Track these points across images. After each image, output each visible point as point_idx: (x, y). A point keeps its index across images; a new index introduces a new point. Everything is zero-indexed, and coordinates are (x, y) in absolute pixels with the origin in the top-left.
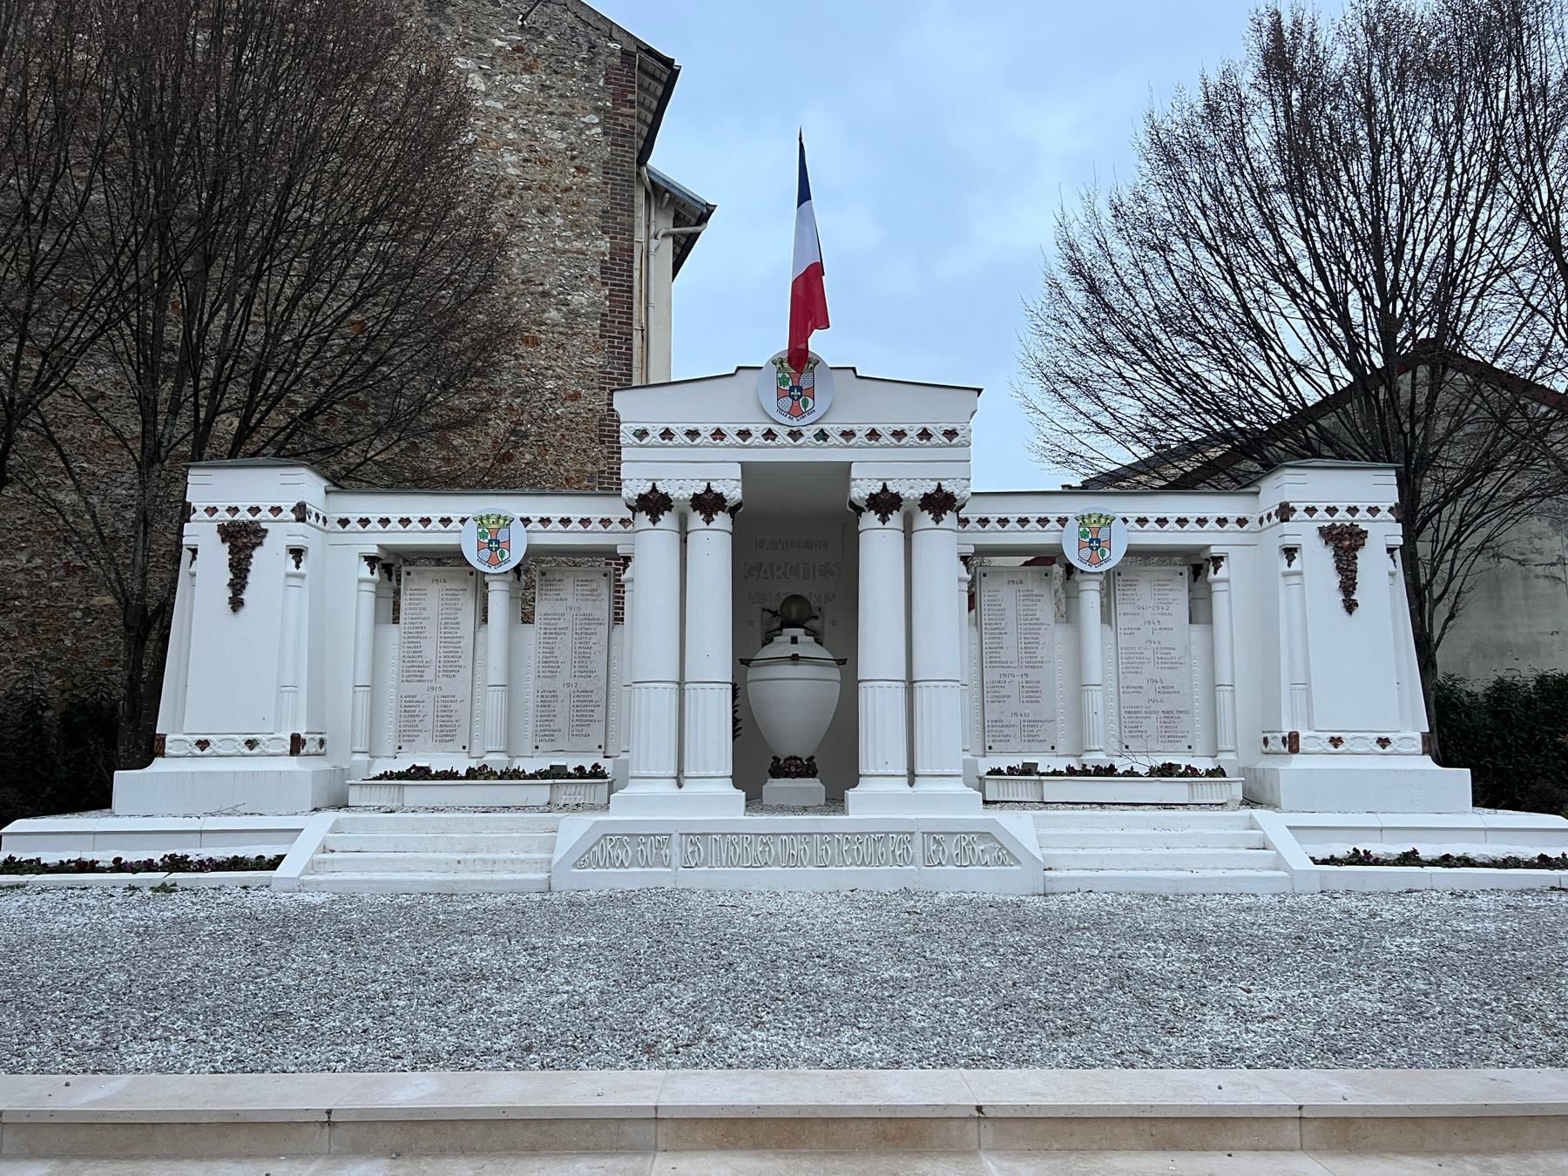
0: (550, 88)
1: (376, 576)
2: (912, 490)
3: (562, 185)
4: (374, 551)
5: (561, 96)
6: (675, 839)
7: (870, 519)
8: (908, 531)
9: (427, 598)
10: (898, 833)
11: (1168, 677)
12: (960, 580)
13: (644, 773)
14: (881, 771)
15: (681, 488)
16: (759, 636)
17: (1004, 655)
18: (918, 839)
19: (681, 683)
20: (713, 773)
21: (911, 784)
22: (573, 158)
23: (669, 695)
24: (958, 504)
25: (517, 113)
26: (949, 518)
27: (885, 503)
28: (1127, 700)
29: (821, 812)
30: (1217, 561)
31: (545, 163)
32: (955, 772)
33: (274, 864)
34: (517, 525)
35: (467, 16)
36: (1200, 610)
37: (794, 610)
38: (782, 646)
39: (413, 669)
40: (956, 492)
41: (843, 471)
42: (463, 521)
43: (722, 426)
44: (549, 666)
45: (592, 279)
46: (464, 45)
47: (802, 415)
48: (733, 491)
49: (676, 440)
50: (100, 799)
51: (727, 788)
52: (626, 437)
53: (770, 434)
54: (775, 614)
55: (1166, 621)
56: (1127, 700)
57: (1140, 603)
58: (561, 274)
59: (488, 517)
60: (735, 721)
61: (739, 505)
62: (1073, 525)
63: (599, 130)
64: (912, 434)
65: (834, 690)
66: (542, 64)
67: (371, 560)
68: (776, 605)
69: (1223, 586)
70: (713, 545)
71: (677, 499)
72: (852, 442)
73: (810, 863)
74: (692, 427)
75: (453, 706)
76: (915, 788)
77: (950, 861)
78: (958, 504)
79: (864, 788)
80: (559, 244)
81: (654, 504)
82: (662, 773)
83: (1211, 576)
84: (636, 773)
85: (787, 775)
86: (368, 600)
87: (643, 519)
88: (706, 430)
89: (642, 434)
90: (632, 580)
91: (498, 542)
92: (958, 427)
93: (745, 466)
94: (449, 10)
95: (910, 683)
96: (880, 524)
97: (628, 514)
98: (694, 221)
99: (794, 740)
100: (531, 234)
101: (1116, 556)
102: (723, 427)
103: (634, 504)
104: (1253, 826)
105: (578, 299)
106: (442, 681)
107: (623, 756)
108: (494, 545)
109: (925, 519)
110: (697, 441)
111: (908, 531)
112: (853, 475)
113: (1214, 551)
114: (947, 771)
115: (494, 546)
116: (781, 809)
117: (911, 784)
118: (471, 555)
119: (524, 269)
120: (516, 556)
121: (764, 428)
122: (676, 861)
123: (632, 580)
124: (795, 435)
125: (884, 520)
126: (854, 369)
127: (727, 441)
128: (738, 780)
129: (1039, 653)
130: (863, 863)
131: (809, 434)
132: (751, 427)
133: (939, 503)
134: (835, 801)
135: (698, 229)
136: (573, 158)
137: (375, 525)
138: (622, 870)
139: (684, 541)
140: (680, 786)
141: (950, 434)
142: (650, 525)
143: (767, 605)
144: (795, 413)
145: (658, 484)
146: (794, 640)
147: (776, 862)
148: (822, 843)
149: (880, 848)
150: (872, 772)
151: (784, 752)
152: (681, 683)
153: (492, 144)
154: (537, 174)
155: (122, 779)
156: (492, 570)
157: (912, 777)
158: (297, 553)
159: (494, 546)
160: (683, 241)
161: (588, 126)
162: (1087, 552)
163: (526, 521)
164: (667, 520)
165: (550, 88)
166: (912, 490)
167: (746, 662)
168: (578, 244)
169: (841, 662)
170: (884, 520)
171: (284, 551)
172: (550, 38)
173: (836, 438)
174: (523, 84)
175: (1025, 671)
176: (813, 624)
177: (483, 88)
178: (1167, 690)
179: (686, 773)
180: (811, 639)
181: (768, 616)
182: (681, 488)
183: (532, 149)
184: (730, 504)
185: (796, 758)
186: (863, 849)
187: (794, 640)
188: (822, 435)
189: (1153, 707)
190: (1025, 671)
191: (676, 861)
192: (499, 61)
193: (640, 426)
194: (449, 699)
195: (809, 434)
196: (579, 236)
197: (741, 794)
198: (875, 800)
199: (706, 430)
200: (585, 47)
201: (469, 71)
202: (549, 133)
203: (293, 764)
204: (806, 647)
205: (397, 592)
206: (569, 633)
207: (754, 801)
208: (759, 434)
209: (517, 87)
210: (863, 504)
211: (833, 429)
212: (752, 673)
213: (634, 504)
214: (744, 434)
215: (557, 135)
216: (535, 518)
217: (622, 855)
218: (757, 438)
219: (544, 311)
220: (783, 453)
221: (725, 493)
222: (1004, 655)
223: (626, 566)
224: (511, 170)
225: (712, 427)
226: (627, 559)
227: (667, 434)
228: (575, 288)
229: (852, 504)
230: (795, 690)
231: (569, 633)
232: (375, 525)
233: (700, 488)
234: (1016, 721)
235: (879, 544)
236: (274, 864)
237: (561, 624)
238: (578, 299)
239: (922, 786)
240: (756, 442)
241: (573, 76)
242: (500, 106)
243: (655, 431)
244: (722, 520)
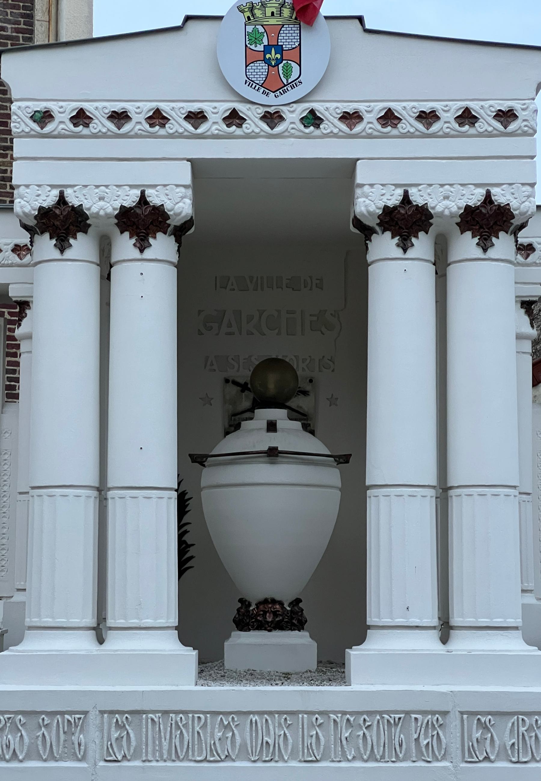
2: (447, 201)
6: (93, 718)
7: (384, 245)
8: (441, 264)
10: (424, 713)
12: (520, 337)
13: (48, 621)
14: (400, 621)
15: (101, 200)
16: (219, 421)
18: (454, 722)
19: (102, 490)
20: (149, 622)
21: (444, 640)
23: (84, 507)
24: (516, 222)
26: (503, 244)
27: (406, 220)
29: (311, 681)
32: (511, 622)
37: (272, 383)
38: (253, 435)
40: (514, 204)
41: (349, 167)
43: (163, 106)
47: (282, 88)
48: (179, 203)
51: (169, 644)
52: (20, 120)
53: (234, 118)
54: (244, 387)
60: (183, 547)
61: (188, 224)
64: (371, 119)
65: (329, 503)
68: (244, 375)
70: (149, 282)
71: (97, 215)
72: (358, 129)
73: (293, 755)
74: (118, 107)
76: (106, 646)
77: (503, 754)
78: (516, 222)
79: (375, 645)
81: (61, 222)
82: (75, 621)
84: (35, 621)
85: (261, 626)
87: (46, 245)
88: (139, 111)
89: (44, 117)
90: (29, 337)
91: (280, 49)
92: (517, 106)
93: (198, 167)
95: (443, 491)
96: (399, 253)
97: (24, 238)
99: (271, 575)
102: (165, 107)
103: (32, 222)
107: (18, 597)
108: (273, 55)
109: (466, 245)
110: (127, 128)
111: (441, 264)
112: (360, 179)
114: (498, 621)
116: (251, 676)
117: (444, 640)
121: (224, 108)
122: (94, 751)
123: (29, 337)
124: (272, 118)
125: (405, 246)
126: (360, 19)
127: (170, 128)
128: (186, 634)
130: (372, 757)
131: (293, 116)
132: (206, 107)
133: (488, 220)
134: (332, 666)
138: (14, 765)
139: (106, 278)
140: (101, 641)
141: (506, 116)
142: (56, 254)
143: (232, 374)
145: (412, 191)
146: (272, 427)
147: (244, 753)
148: (312, 726)
149: (398, 734)
150: (386, 621)
151: (256, 593)
152: (102, 490)
157: (445, 630)
164: (82, 246)
166: (447, 201)
167: (200, 460)
169: (342, 460)
170: (405, 246)
173: (332, 124)
176: (297, 402)
179: (110, 622)
180: (298, 425)
181: (234, 390)
182: (101, 200)
184: (174, 222)
185: (274, 601)
186: (371, 736)
187: (272, 427)
188: (313, 119)
191: (94, 751)
193: (41, 106)
195: (293, 116)
197: (192, 654)
198: (390, 664)
199: (139, 111)
204: (291, 436)
207: (210, 664)
208: (218, 118)
210: (373, 222)
211: (329, 109)
212: (210, 476)
213: (32, 222)
214: (196, 118)
217: (14, 742)
218: (214, 124)
220: (254, 146)
221: (168, 205)
223: (21, 315)
225: (148, 108)
226: (24, 305)
229: (358, 223)
230: (272, 503)
233: (130, 199)
235: (398, 282)
239: (461, 643)
240: (214, 130)
244: (163, 246)
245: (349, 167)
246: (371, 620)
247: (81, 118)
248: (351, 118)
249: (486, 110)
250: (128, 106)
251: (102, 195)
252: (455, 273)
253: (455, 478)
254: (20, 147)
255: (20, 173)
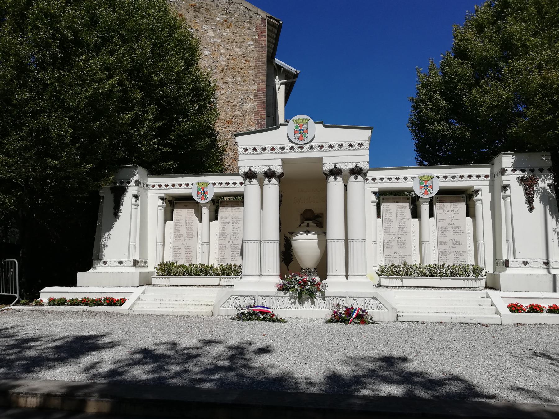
0: (236, 33)
1: (164, 204)
3: (241, 67)
4: (163, 195)
5: (240, 36)
9: (183, 214)
11: (457, 238)
12: (373, 202)
17: (392, 230)
21: (347, 278)
22: (244, 57)
24: (364, 172)
25: (225, 43)
27: (336, 172)
28: (442, 247)
30: (477, 192)
31: (235, 59)
33: (121, 302)
34: (211, 186)
35: (207, 11)
36: (471, 213)
39: (177, 237)
41: (321, 159)
42: (193, 184)
44: (223, 235)
45: (251, 99)
46: (206, 21)
47: (303, 139)
48: (278, 170)
49: (258, 152)
50: (72, 283)
52: (240, 151)
53: (292, 148)
55: (456, 216)
56: (442, 247)
57: (446, 209)
58: (240, 98)
59: (424, 176)
61: (282, 175)
62: (417, 180)
63: (253, 47)
64: (326, 147)
66: (233, 25)
67: (163, 199)
69: (480, 202)
70: (272, 189)
75: (191, 250)
80: (239, 88)
81: (250, 176)
83: (475, 198)
86: (161, 212)
89: (246, 150)
91: (303, 130)
93: (283, 160)
94: (201, 9)
98: (292, 77)
100: (230, 84)
101: (435, 191)
104: (488, 297)
105: (246, 107)
106: (187, 241)
108: (301, 132)
112: (323, 162)
113: (475, 188)
115: (426, 187)
117: (347, 278)
118: (195, 197)
119: (227, 97)
120: (210, 197)
127: (276, 151)
129: (405, 229)
131: (307, 147)
132: (285, 146)
135: (294, 80)
136: (244, 57)
137: (163, 187)
144: (301, 139)
145: (251, 168)
153: (216, 54)
154: (232, 64)
155: (80, 275)
156: (202, 202)
157: (347, 276)
158: (136, 197)
159: (203, 193)
160: (289, 85)
161: (250, 45)
162: (423, 190)
163: (214, 184)
165: (236, 33)
168: (246, 87)
171: (131, 196)
172: (236, 16)
173: (317, 148)
174: (226, 33)
175: (399, 236)
177: (213, 35)
178: (458, 243)
183: (230, 55)
184: (277, 174)
188: (311, 147)
189: (452, 250)
190: (399, 236)
192: (219, 25)
194: (190, 247)
195: (307, 147)
196: (246, 85)
199: (269, 148)
200: (248, 17)
201: (208, 30)
202: (236, 49)
203: (133, 270)
205: (173, 210)
206: (230, 223)
209: (225, 34)
214: (283, 148)
215: (238, 49)
216: (216, 184)
218: (287, 149)
219: (234, 112)
222: (392, 230)
224: (223, 63)
227: (255, 149)
228: (245, 103)
230: (306, 243)
231: (230, 223)
232: (163, 187)
233: (266, 169)
234: (396, 255)
235: (335, 187)
236: (121, 302)
237: (227, 220)
238: (246, 107)
241: (244, 28)
242: (219, 41)
243: (250, 149)
245: (321, 159)
246: (328, 273)
247: (273, 149)
248: (322, 147)
249: (355, 144)
250: (284, 145)
251: (260, 168)
252: (265, 187)
253: (349, 237)
254: (240, 157)
255: (240, 164)
